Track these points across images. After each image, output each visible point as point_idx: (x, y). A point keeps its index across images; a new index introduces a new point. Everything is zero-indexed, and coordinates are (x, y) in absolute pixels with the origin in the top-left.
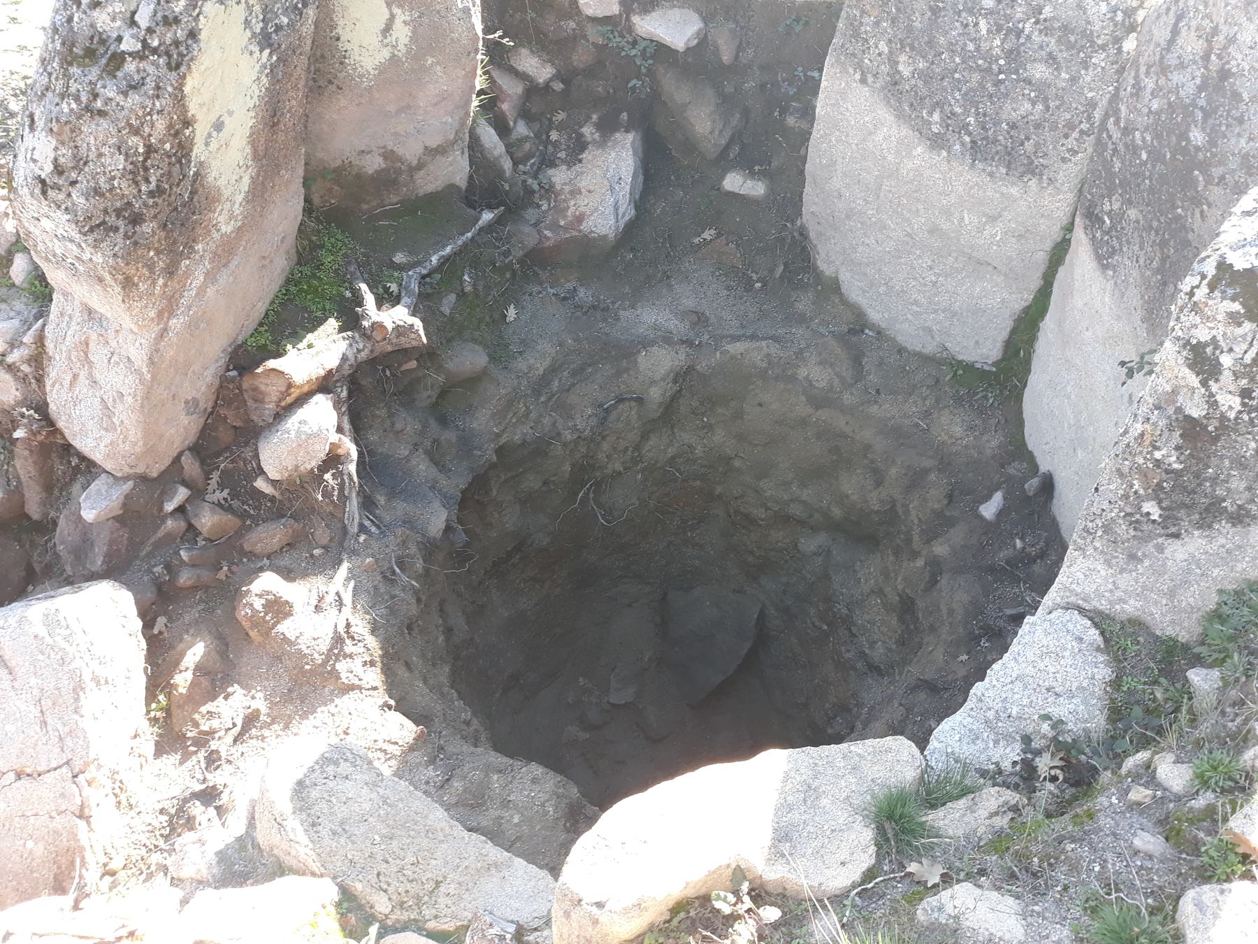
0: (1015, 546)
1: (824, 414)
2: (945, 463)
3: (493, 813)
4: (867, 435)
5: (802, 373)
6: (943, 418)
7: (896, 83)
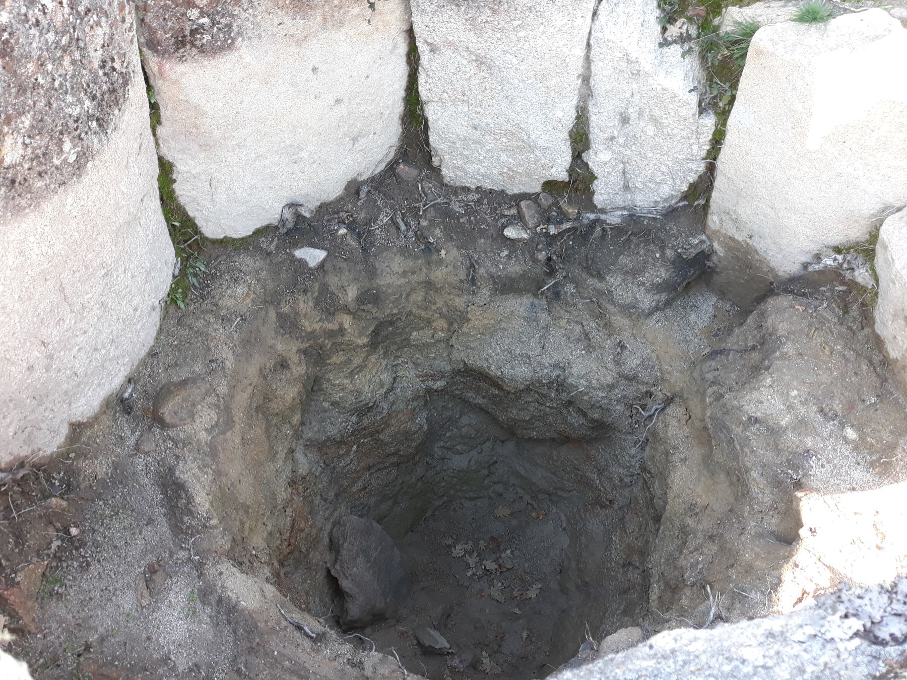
0: (344, 235)
1: (238, 414)
2: (272, 299)
3: (802, 410)
4: (252, 370)
5: (203, 436)
6: (229, 304)
7: (13, 182)
